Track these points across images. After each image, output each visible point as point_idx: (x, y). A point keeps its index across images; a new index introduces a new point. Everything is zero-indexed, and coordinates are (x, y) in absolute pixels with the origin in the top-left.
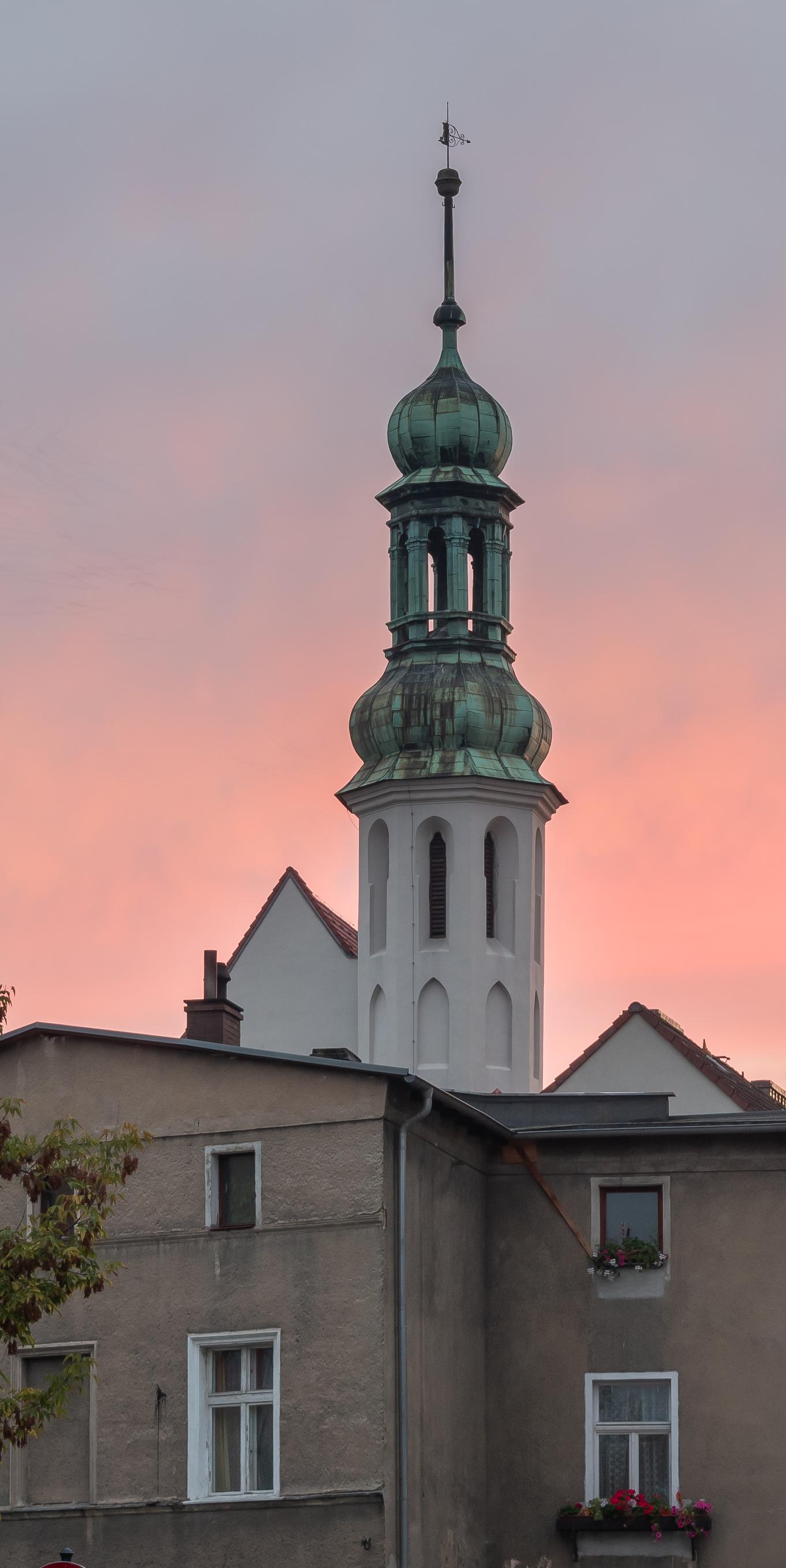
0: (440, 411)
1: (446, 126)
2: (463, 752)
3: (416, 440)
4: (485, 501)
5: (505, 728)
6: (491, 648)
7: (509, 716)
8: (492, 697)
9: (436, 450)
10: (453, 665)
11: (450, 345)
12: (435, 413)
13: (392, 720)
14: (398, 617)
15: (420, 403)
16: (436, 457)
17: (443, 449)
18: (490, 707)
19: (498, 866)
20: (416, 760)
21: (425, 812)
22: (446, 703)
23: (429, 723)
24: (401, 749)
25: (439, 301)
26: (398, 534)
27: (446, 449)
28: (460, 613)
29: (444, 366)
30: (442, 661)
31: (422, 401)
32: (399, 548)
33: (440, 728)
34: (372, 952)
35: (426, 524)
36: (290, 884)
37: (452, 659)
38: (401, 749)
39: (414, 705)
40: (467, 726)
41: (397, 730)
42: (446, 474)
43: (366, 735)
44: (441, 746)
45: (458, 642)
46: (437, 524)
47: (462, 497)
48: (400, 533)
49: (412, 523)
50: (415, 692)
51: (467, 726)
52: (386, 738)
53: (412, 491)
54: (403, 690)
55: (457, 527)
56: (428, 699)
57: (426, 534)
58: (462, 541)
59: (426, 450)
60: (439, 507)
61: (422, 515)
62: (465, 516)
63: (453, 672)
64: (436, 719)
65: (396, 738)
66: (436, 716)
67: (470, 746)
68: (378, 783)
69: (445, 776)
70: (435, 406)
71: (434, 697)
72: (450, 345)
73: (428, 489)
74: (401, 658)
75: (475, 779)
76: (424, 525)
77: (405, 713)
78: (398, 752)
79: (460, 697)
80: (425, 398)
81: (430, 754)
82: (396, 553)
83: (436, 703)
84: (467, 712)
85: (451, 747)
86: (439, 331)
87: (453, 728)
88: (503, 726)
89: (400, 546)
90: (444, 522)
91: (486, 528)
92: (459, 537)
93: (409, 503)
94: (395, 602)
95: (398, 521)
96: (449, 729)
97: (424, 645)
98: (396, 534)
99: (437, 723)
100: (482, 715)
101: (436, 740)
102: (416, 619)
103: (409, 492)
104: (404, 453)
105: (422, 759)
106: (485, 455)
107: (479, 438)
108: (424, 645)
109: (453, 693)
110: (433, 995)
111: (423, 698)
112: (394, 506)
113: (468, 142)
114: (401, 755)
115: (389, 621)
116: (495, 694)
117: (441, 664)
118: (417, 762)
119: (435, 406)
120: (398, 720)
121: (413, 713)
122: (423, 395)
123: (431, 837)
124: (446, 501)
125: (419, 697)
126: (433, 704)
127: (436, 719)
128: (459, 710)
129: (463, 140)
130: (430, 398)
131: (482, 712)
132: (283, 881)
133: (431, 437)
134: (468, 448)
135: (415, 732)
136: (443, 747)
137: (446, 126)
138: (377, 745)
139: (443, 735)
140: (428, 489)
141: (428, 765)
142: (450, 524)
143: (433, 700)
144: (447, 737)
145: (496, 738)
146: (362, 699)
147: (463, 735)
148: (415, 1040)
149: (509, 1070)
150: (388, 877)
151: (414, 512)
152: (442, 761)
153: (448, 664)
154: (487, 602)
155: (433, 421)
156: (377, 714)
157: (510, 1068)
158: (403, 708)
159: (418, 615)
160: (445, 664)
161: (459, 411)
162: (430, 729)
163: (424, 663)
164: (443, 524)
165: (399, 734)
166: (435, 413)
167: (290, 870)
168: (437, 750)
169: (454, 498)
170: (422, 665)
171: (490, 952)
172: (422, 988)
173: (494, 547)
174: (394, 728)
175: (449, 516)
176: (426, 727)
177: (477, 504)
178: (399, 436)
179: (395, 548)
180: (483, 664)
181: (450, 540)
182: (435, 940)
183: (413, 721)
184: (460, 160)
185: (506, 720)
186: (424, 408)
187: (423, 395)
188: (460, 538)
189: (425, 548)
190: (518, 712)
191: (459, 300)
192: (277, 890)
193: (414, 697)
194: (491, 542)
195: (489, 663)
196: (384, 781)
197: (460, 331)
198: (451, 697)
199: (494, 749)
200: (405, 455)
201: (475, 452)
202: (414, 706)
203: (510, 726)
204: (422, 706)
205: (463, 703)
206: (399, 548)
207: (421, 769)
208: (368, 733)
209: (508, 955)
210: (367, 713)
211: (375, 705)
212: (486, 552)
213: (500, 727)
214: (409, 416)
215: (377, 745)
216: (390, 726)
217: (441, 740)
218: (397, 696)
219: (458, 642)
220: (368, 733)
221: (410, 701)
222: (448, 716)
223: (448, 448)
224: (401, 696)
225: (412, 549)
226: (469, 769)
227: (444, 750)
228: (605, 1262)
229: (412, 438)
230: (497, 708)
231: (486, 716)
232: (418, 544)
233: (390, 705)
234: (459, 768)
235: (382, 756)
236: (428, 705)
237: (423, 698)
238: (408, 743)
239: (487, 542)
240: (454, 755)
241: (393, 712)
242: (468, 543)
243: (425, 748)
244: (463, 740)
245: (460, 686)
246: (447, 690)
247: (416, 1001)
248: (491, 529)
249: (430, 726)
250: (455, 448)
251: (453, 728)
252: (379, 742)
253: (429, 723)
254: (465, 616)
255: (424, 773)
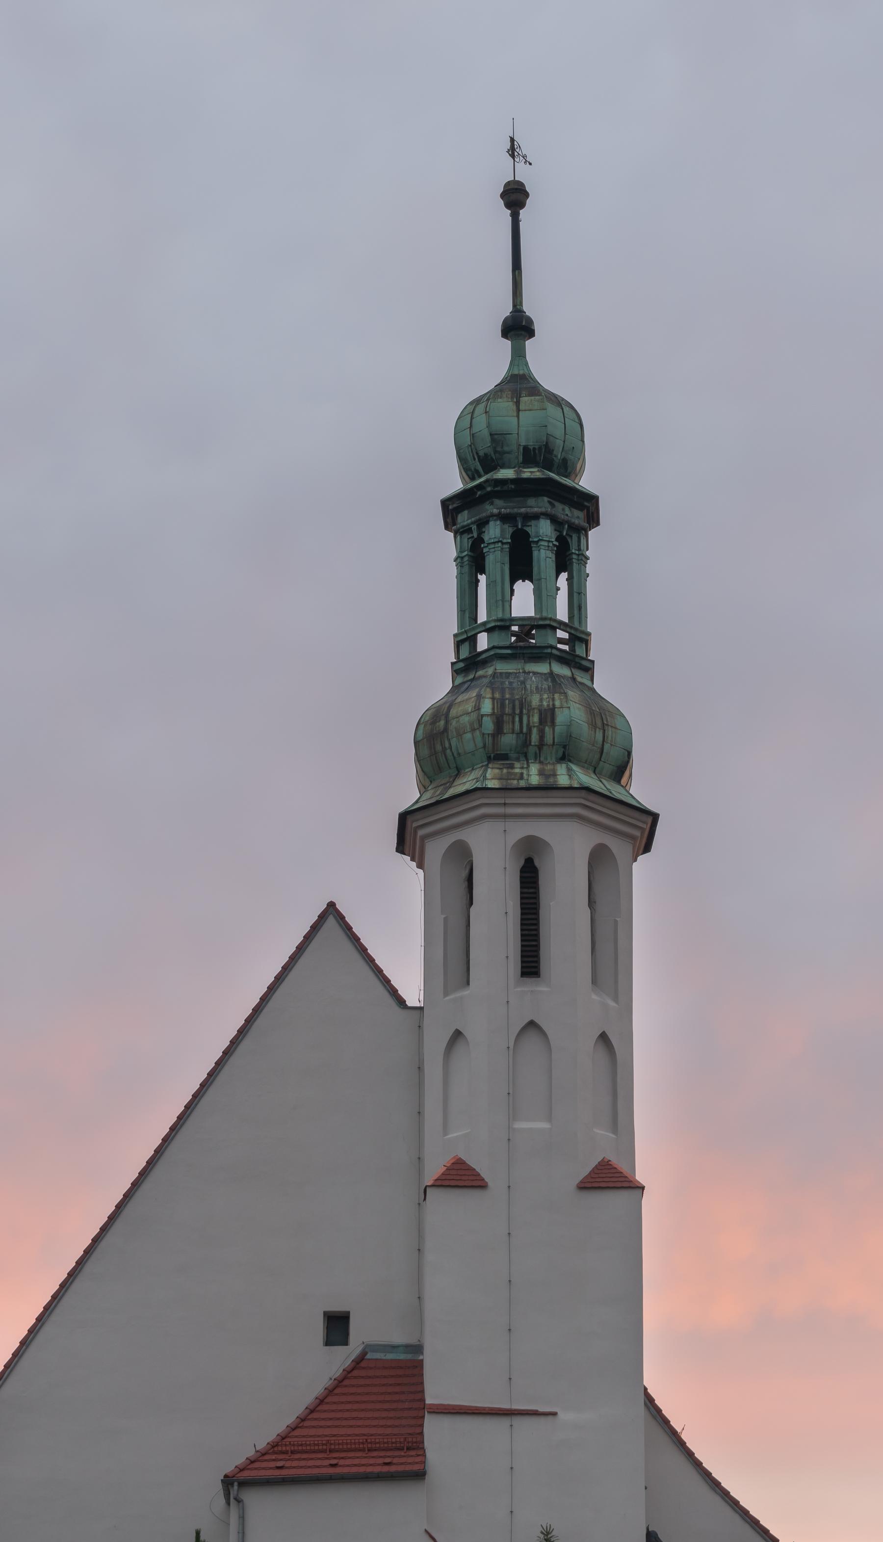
0: (523, 409)
1: (512, 140)
2: (564, 766)
3: (496, 436)
4: (571, 508)
5: (607, 746)
6: (581, 664)
7: (610, 733)
8: (593, 710)
9: (518, 449)
10: (545, 674)
11: (519, 354)
12: (518, 410)
13: (481, 726)
14: (469, 626)
15: (499, 400)
16: (517, 458)
17: (526, 449)
18: (592, 720)
19: (595, 902)
20: (510, 770)
21: (520, 830)
22: (545, 710)
23: (525, 730)
24: (489, 759)
25: (507, 310)
26: (468, 539)
27: (531, 449)
28: (551, 619)
29: (516, 372)
30: (530, 670)
31: (501, 398)
32: (470, 553)
33: (538, 737)
34: (446, 994)
35: (508, 525)
36: (331, 921)
37: (543, 668)
38: (489, 759)
39: (507, 709)
40: (569, 736)
41: (487, 737)
42: (531, 473)
43: (439, 748)
44: (537, 758)
45: (549, 651)
46: (522, 526)
47: (550, 500)
48: (473, 537)
49: (491, 523)
50: (507, 696)
51: (570, 736)
52: (470, 747)
53: (494, 488)
54: (493, 693)
55: (544, 529)
56: (524, 704)
57: (508, 535)
58: (551, 545)
59: (506, 449)
60: (524, 507)
61: (504, 514)
62: (554, 520)
63: (546, 680)
64: (534, 726)
65: (484, 747)
66: (533, 723)
67: (570, 761)
68: (467, 792)
69: (548, 788)
70: (518, 403)
71: (531, 702)
72: (519, 354)
73: (513, 487)
74: (476, 669)
75: (583, 793)
76: (506, 526)
77: (498, 718)
78: (486, 763)
79: (561, 704)
80: (505, 396)
81: (525, 766)
82: (466, 559)
83: (534, 709)
84: (571, 721)
85: (549, 760)
86: (507, 344)
87: (554, 738)
88: (605, 744)
89: (470, 551)
90: (529, 524)
91: (571, 537)
92: (547, 539)
93: (488, 502)
94: (464, 611)
95: (472, 523)
96: (548, 739)
97: (509, 651)
98: (466, 540)
99: (535, 731)
100: (585, 727)
101: (532, 750)
102: (499, 624)
103: (489, 489)
104: (477, 454)
105: (517, 771)
106: (569, 462)
107: (564, 441)
108: (509, 651)
109: (553, 700)
110: (532, 1041)
111: (517, 703)
112: (463, 510)
113: (530, 164)
114: (490, 765)
115: (456, 632)
116: (595, 708)
117: (529, 672)
118: (510, 772)
119: (518, 403)
120: (489, 725)
121: (506, 718)
122: (501, 394)
123: (522, 862)
124: (531, 501)
125: (512, 701)
126: (530, 709)
127: (534, 726)
128: (561, 717)
129: (526, 160)
130: (510, 396)
131: (584, 723)
132: (322, 917)
133: (513, 435)
134: (553, 450)
135: (508, 740)
136: (540, 760)
137: (512, 140)
138: (454, 758)
139: (541, 745)
140: (513, 487)
141: (525, 776)
142: (536, 526)
143: (530, 705)
144: (545, 748)
145: (597, 756)
146: (430, 712)
147: (564, 747)
148: (511, 1092)
149: (616, 1137)
150: (472, 904)
151: (495, 511)
152: (541, 773)
153: (538, 673)
154: (574, 616)
155: (516, 419)
156: (458, 722)
157: (617, 1135)
158: (494, 712)
159: (502, 620)
160: (535, 673)
161: (546, 409)
162: (526, 737)
163: (510, 671)
164: (529, 526)
165: (489, 740)
166: (518, 410)
167: (331, 905)
168: (532, 763)
169: (540, 499)
170: (507, 673)
171: (594, 997)
172: (522, 1026)
173: (580, 558)
174: (483, 734)
175: (536, 517)
176: (521, 735)
177: (563, 510)
178: (473, 436)
179: (466, 553)
180: (573, 679)
181: (537, 542)
182: (527, 980)
183: (507, 728)
184: (524, 174)
185: (607, 737)
186: (505, 405)
187: (501, 394)
188: (549, 541)
189: (508, 550)
190: (619, 731)
191: (528, 308)
192: (315, 928)
193: (507, 701)
194: (577, 552)
195: (579, 679)
196: (476, 789)
197: (529, 344)
198: (551, 703)
199: (593, 769)
200: (479, 457)
201: (559, 456)
202: (508, 710)
203: (611, 745)
204: (518, 711)
205: (566, 711)
206: (470, 553)
207: (518, 780)
208: (442, 744)
209: (612, 1003)
210: (442, 723)
211: (453, 712)
212: (572, 563)
213: (601, 743)
214: (486, 412)
215: (454, 758)
216: (478, 732)
217: (538, 752)
218: (487, 699)
219: (549, 651)
220: (442, 744)
221: (503, 705)
222: (549, 724)
223: (531, 448)
224: (491, 700)
225: (493, 550)
226: (576, 781)
227: (541, 762)
228: (230, 1486)
229: (491, 435)
230: (599, 723)
231: (589, 729)
232: (500, 544)
233: (478, 708)
234: (563, 780)
235: (459, 772)
236: (524, 710)
237: (517, 703)
238: (498, 752)
239: (573, 551)
240: (554, 768)
241: (482, 716)
242: (555, 549)
243: (518, 760)
244: (564, 753)
245: (561, 693)
246: (545, 696)
247: (511, 1047)
248: (576, 538)
249: (526, 734)
250: (540, 448)
251: (554, 738)
252: (459, 754)
253: (525, 730)
254: (555, 624)
255: (522, 784)
